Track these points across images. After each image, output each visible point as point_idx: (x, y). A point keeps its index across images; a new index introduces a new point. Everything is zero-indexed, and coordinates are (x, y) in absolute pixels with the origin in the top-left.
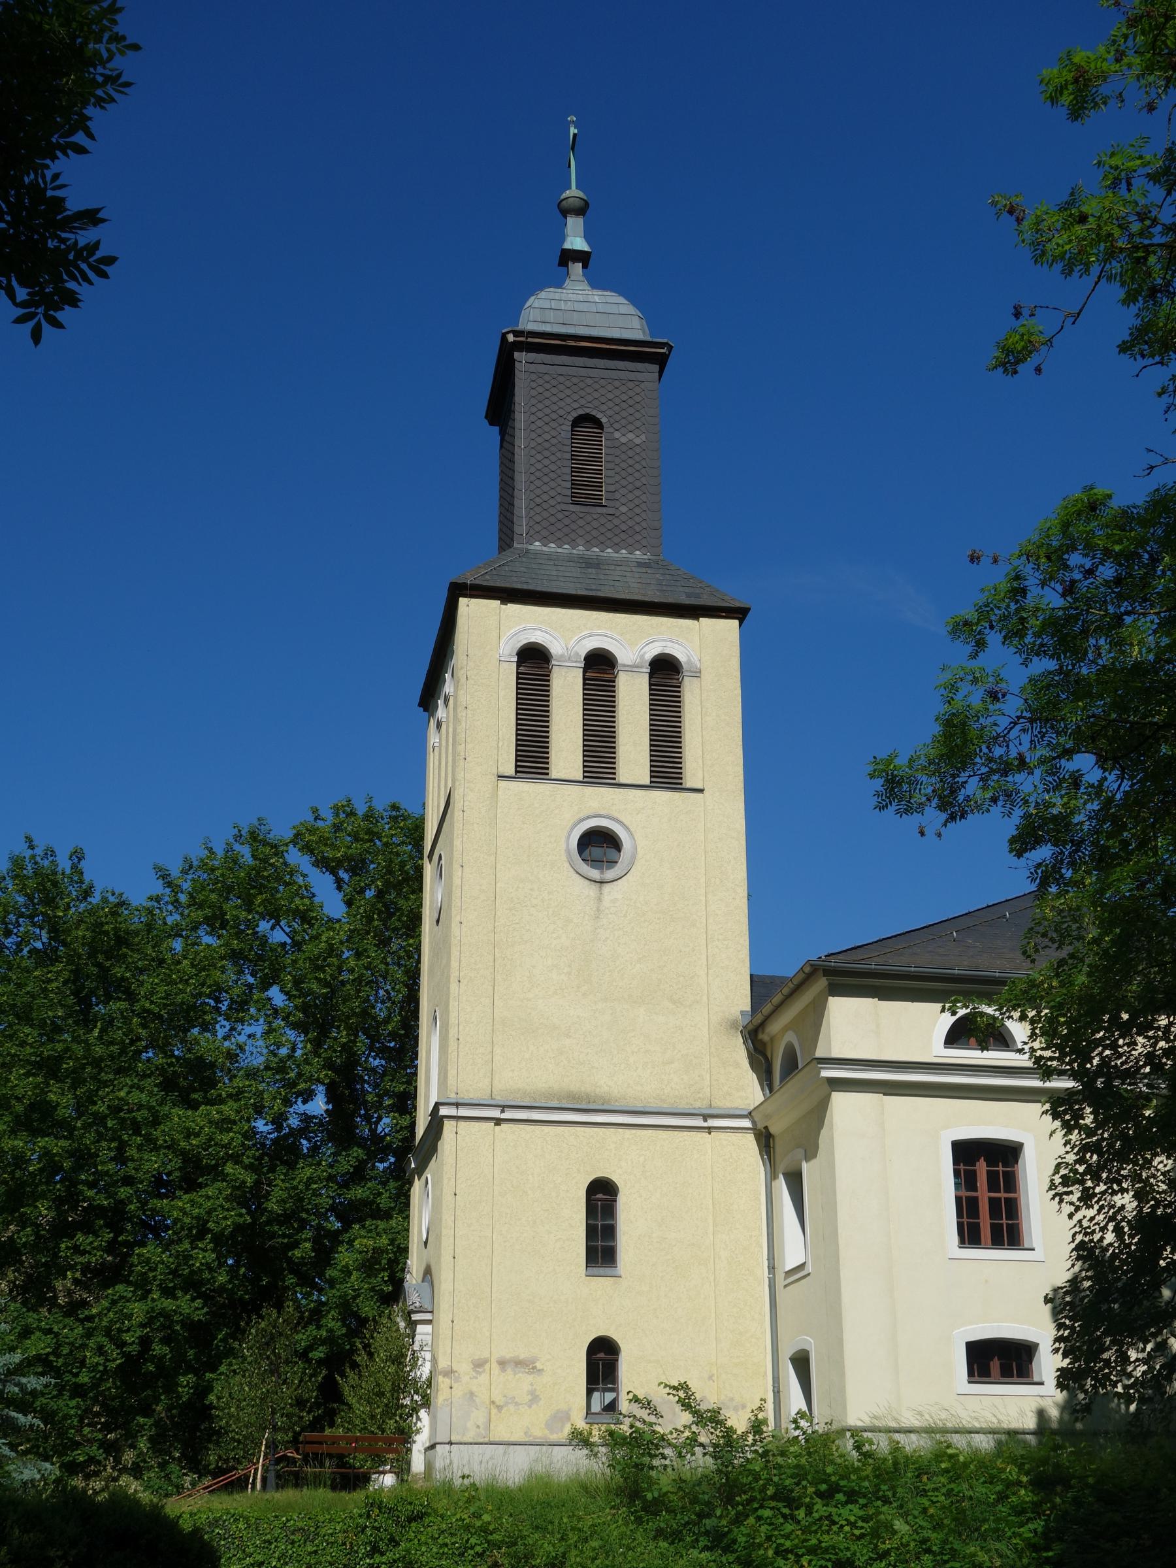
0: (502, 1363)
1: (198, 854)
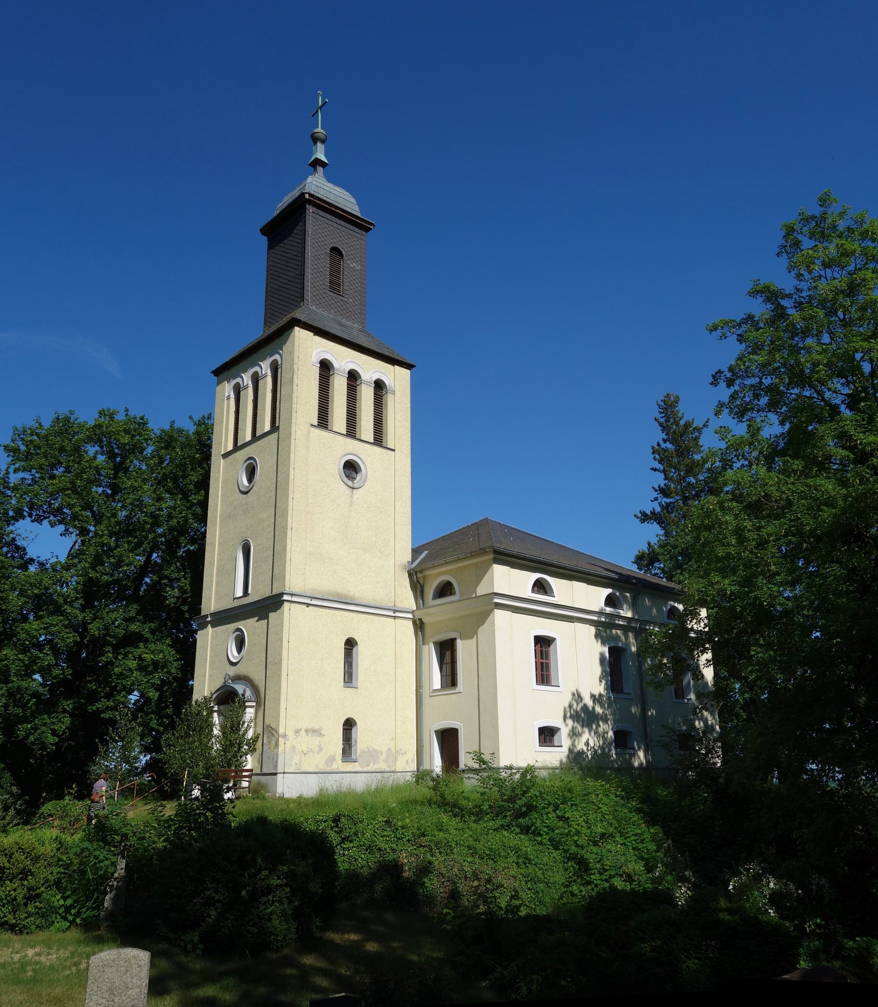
0: (307, 731)
1: (31, 424)
